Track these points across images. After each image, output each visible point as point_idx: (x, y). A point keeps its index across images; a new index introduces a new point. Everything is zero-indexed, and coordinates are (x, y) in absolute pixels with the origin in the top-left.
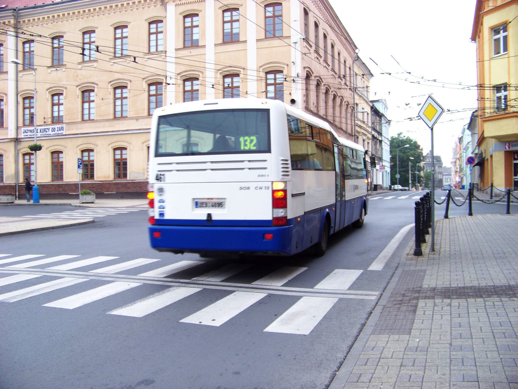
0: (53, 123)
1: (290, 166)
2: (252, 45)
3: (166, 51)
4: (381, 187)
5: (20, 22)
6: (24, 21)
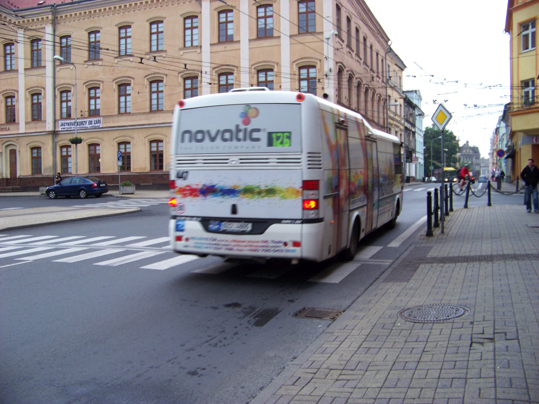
0: (90, 116)
2: (285, 42)
3: (201, 46)
4: (414, 179)
5: (57, 17)
6: (62, 17)
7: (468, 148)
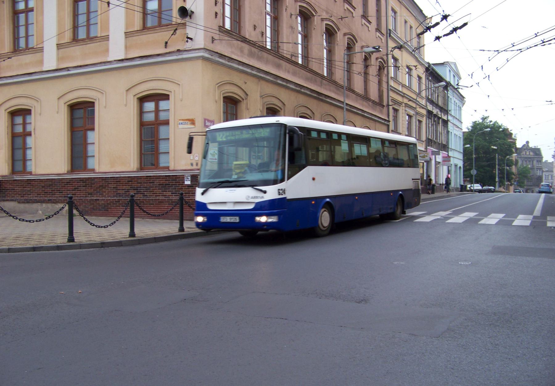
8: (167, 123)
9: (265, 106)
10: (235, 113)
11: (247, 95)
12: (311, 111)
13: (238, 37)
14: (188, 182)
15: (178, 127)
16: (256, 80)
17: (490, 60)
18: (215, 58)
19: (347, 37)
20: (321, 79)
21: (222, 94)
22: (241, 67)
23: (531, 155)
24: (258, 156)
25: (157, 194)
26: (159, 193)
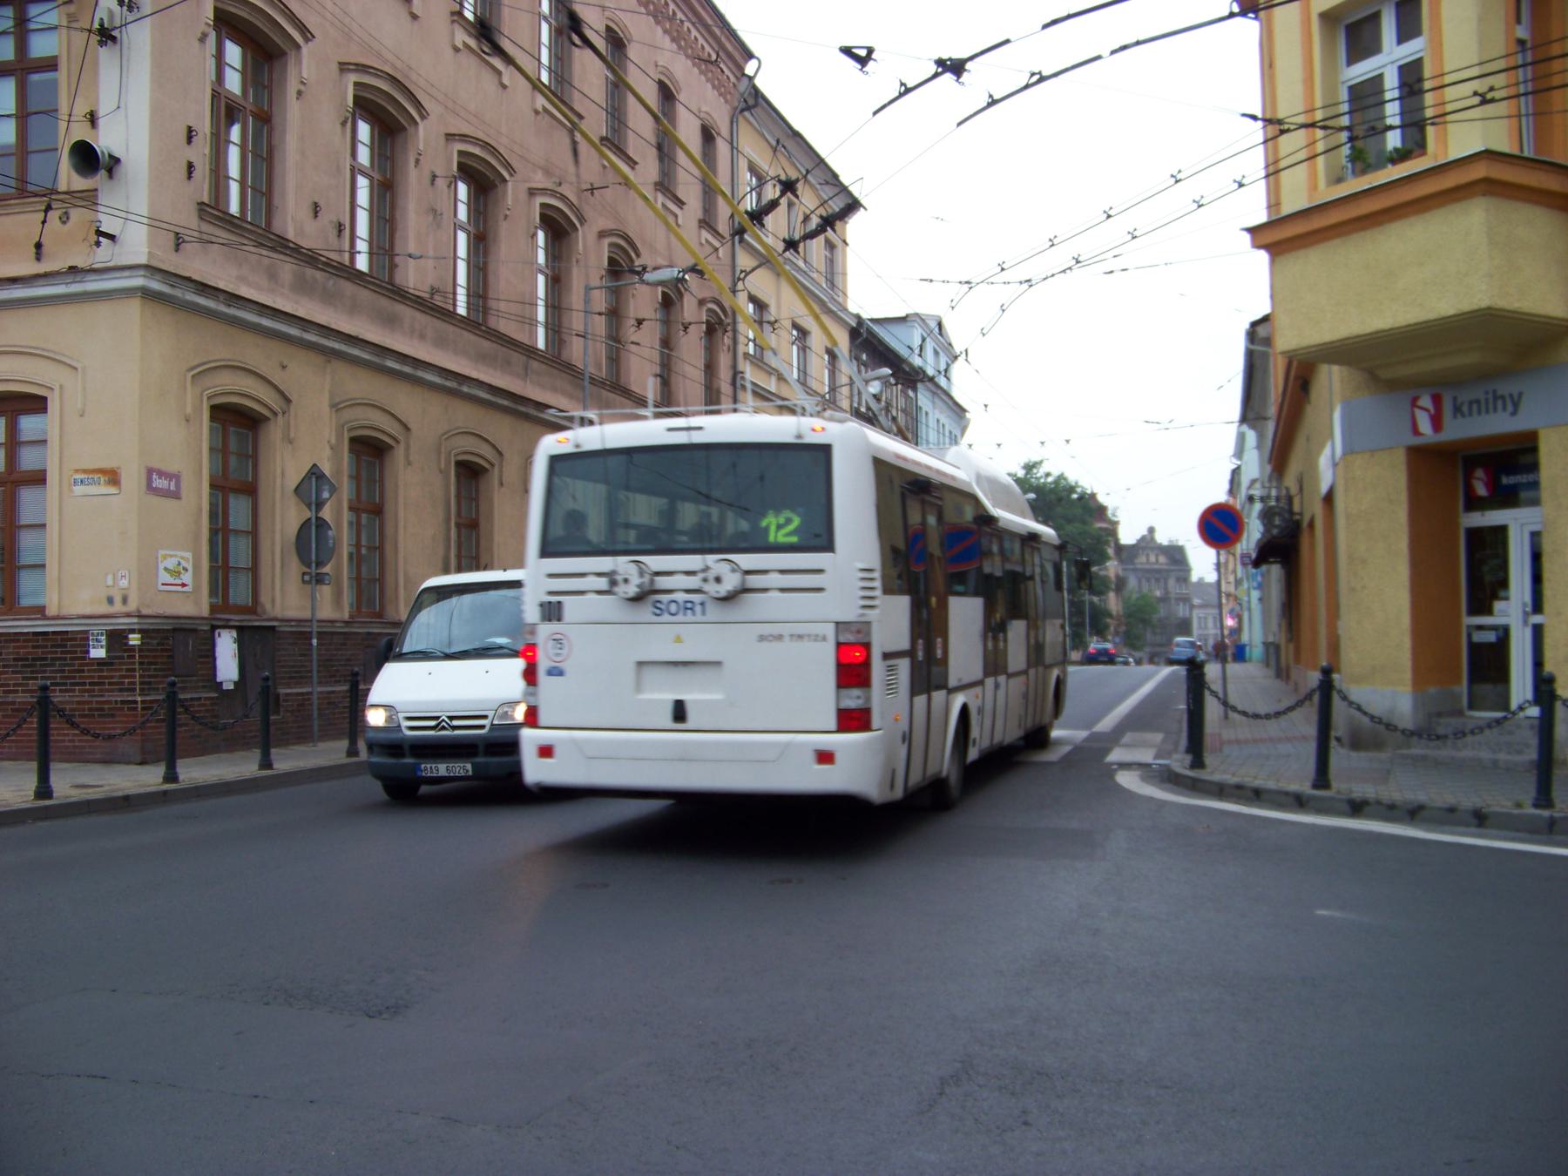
1: (877, 584)
7: (1152, 549)
8: (39, 479)
9: (346, 433)
10: (250, 453)
11: (288, 401)
12: (494, 446)
13: (260, 234)
14: (98, 652)
15: (71, 491)
16: (318, 360)
17: (953, 308)
18: (183, 294)
19: (607, 241)
20: (524, 358)
21: (205, 398)
22: (267, 322)
23: (1161, 564)
24: (318, 574)
25: (8, 685)
26: (15, 685)
